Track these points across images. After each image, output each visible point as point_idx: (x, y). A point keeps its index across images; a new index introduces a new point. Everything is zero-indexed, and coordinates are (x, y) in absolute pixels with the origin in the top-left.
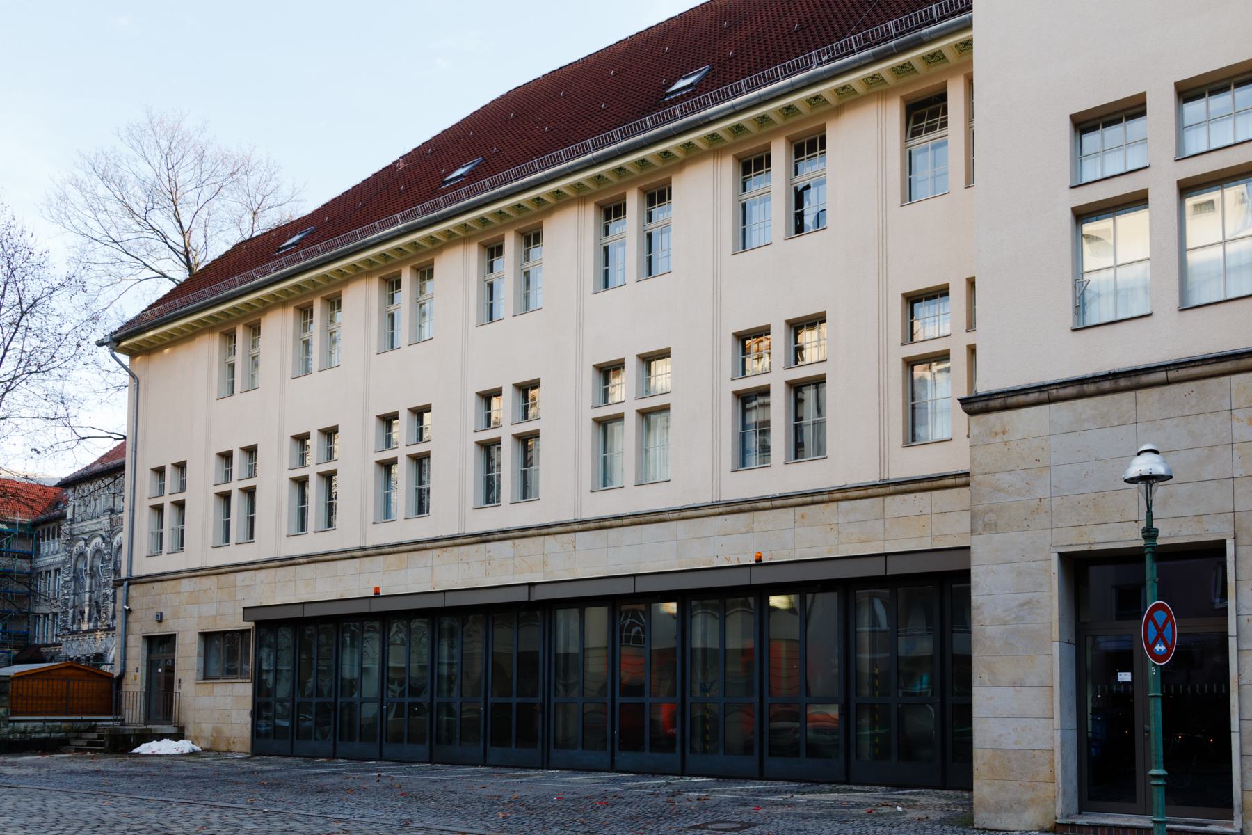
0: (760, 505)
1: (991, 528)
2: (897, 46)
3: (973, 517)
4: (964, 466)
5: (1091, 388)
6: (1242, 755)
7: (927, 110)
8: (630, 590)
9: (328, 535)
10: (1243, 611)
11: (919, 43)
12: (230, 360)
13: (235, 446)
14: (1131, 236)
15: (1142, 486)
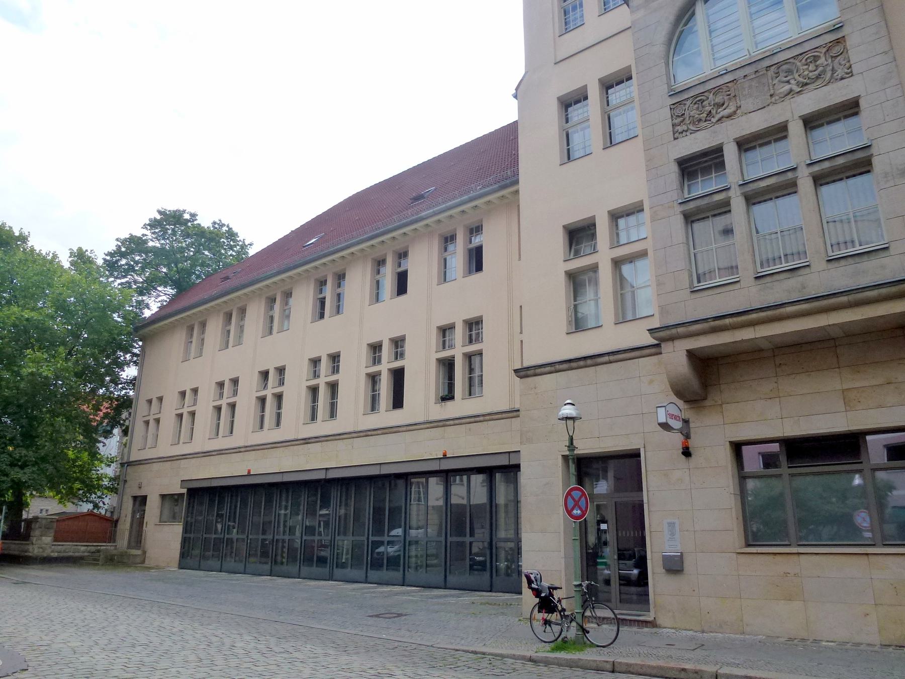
0: (448, 423)
3: (521, 435)
6: (653, 573)
8: (378, 473)
9: (398, 412)
11: (422, 219)
12: (271, 313)
13: (188, 388)
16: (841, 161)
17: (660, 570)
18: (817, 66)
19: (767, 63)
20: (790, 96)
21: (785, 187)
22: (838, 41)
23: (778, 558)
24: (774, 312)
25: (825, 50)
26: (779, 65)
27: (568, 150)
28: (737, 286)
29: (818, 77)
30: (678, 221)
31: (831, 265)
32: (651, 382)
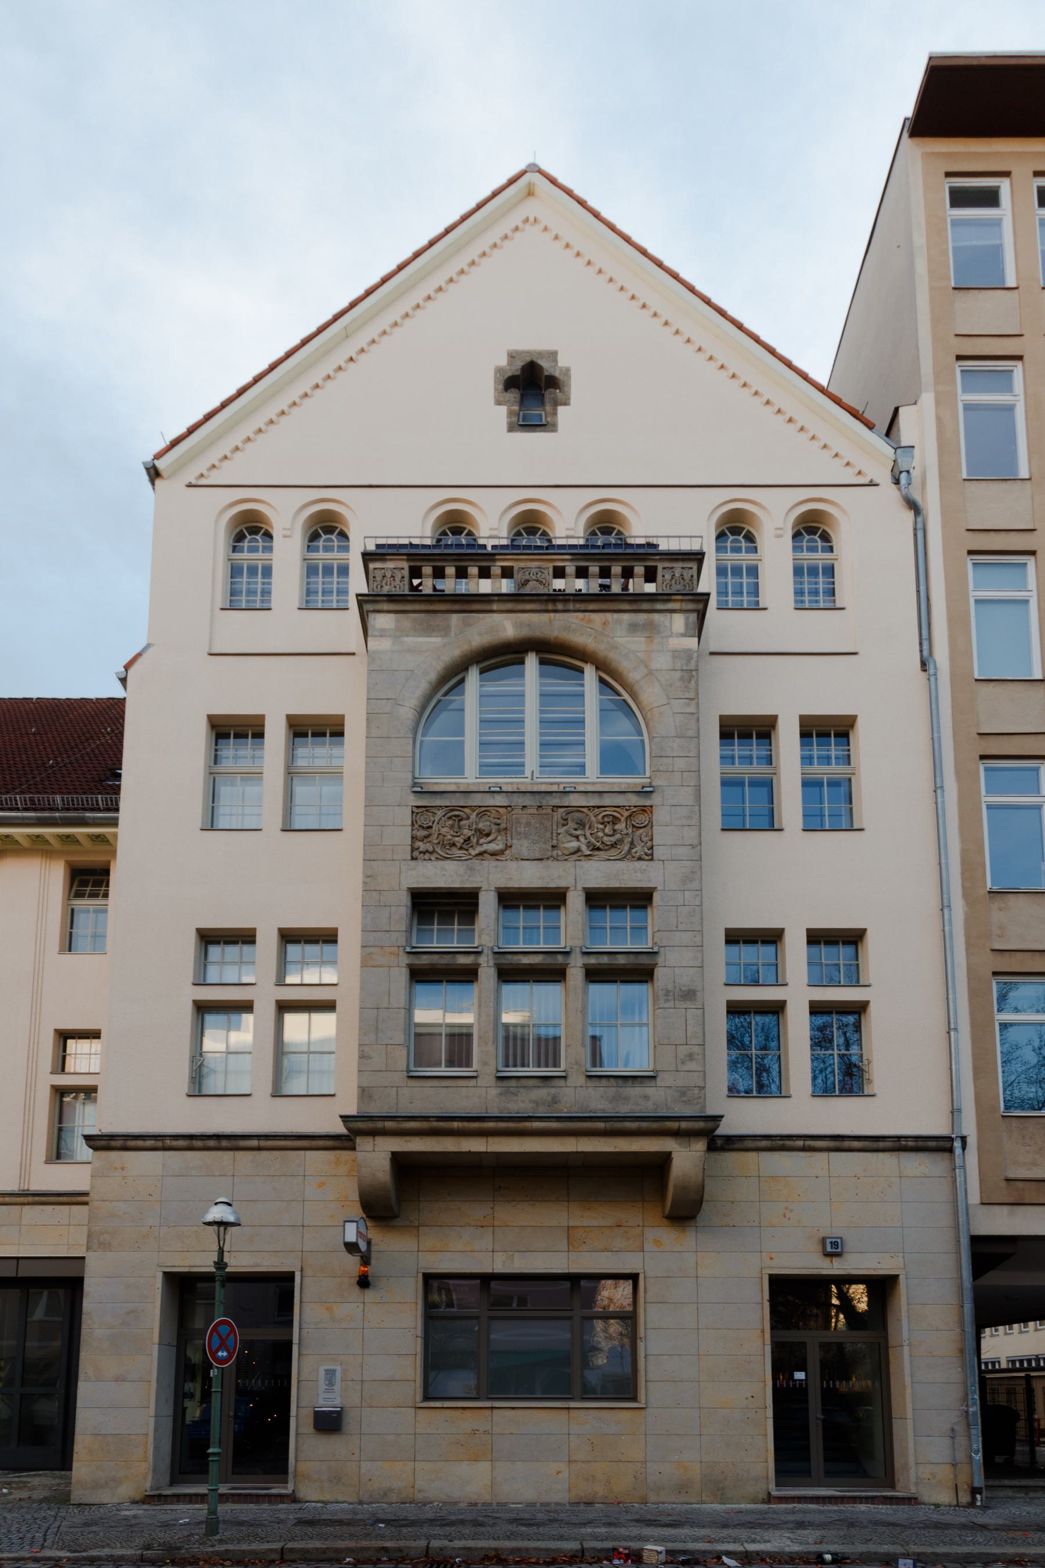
1: (105, 1246)
2: (61, 818)
4: (84, 1187)
5: (199, 1143)
6: (297, 1434)
7: (92, 878)
10: (304, 1326)
14: (245, 1033)
15: (215, 1228)
16: (621, 960)
17: (308, 1427)
18: (615, 831)
19: (555, 801)
20: (575, 857)
21: (551, 972)
22: (644, 809)
23: (468, 1413)
24: (515, 1126)
25: (626, 814)
26: (571, 809)
27: (213, 808)
28: (472, 1082)
29: (613, 846)
30: (401, 976)
31: (590, 1083)
32: (321, 1185)
